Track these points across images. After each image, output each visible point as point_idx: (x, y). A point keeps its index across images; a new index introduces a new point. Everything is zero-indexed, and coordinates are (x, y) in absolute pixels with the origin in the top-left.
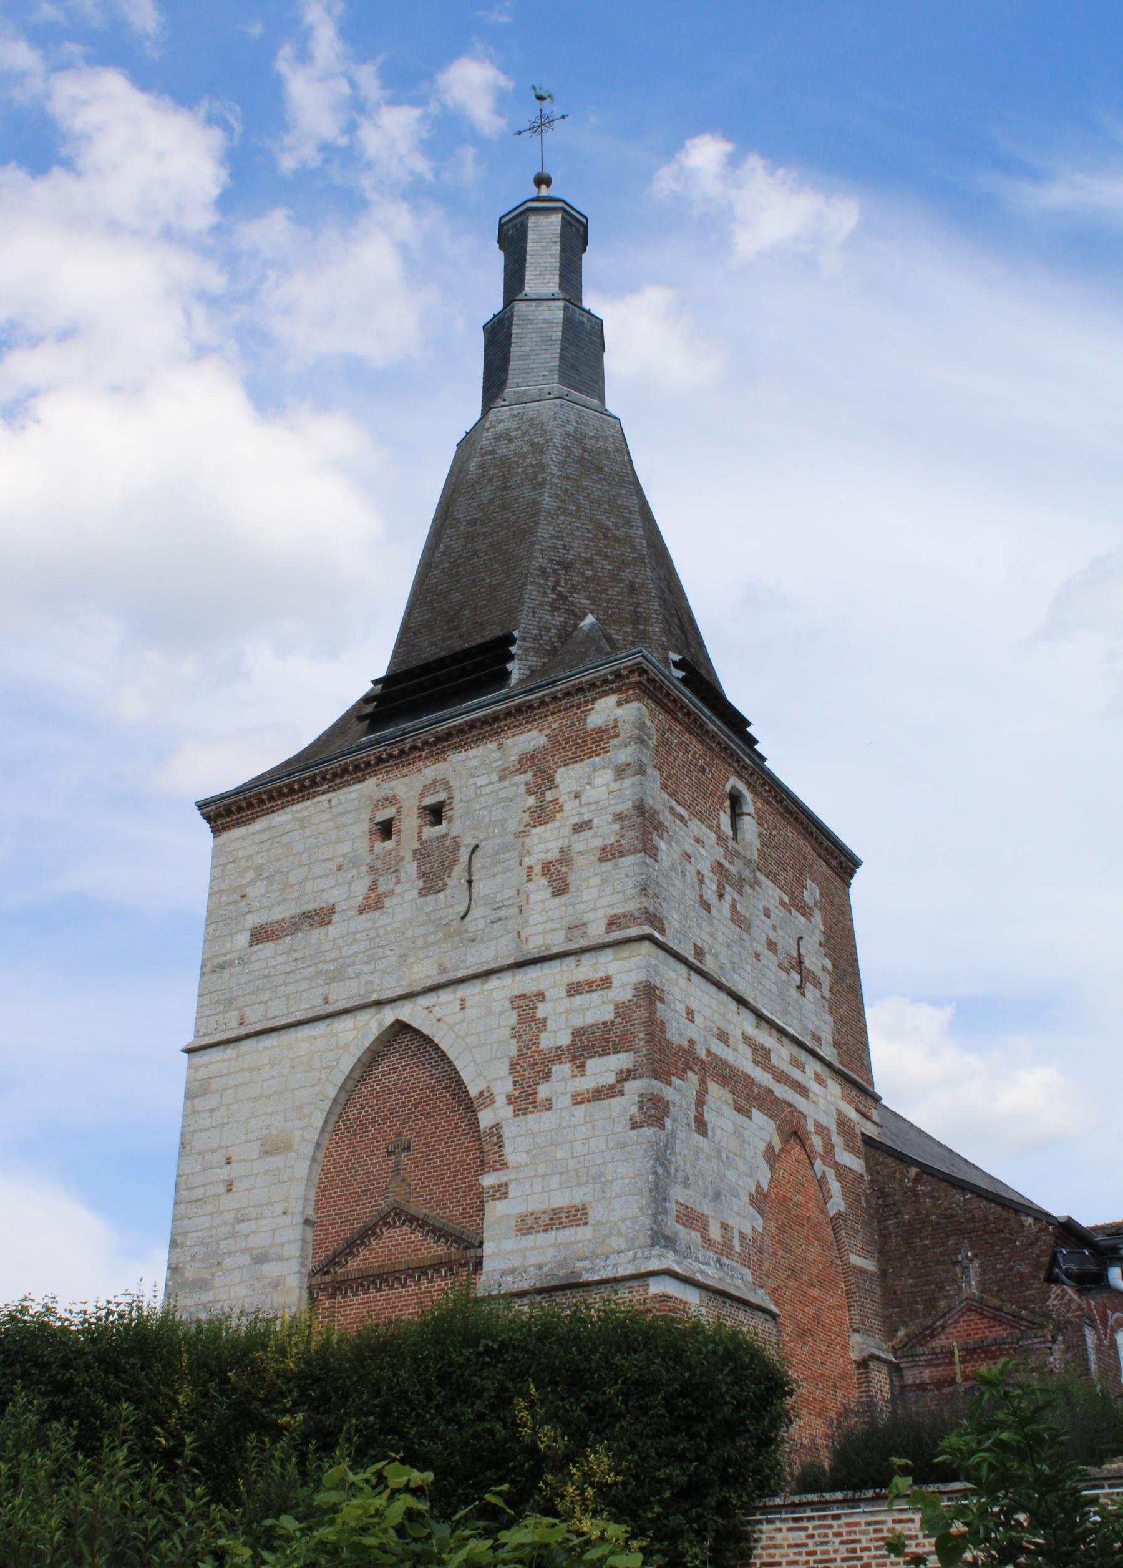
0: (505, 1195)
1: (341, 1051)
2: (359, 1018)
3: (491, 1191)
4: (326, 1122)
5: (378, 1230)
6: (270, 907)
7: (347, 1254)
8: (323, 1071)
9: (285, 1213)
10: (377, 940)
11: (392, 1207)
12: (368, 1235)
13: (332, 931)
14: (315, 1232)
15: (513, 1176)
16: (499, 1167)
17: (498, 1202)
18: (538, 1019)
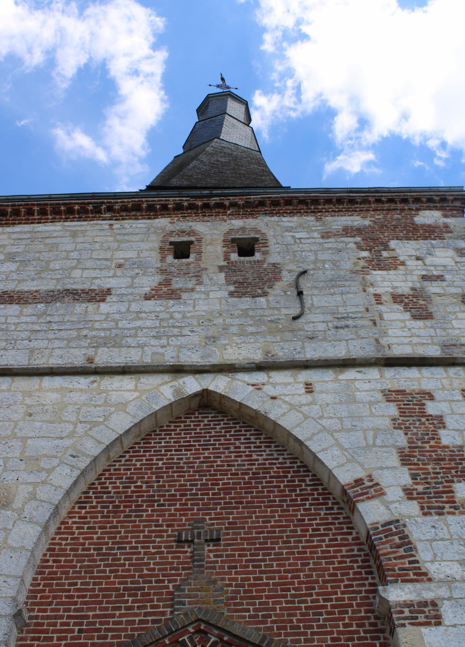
1: (113, 409)
2: (142, 380)
3: (406, 610)
4: (75, 483)
6: (20, 281)
8: (79, 425)
10: (171, 321)
11: (193, 618)
13: (104, 307)
15: (443, 592)
16: (412, 577)
17: (424, 630)
18: (430, 415)
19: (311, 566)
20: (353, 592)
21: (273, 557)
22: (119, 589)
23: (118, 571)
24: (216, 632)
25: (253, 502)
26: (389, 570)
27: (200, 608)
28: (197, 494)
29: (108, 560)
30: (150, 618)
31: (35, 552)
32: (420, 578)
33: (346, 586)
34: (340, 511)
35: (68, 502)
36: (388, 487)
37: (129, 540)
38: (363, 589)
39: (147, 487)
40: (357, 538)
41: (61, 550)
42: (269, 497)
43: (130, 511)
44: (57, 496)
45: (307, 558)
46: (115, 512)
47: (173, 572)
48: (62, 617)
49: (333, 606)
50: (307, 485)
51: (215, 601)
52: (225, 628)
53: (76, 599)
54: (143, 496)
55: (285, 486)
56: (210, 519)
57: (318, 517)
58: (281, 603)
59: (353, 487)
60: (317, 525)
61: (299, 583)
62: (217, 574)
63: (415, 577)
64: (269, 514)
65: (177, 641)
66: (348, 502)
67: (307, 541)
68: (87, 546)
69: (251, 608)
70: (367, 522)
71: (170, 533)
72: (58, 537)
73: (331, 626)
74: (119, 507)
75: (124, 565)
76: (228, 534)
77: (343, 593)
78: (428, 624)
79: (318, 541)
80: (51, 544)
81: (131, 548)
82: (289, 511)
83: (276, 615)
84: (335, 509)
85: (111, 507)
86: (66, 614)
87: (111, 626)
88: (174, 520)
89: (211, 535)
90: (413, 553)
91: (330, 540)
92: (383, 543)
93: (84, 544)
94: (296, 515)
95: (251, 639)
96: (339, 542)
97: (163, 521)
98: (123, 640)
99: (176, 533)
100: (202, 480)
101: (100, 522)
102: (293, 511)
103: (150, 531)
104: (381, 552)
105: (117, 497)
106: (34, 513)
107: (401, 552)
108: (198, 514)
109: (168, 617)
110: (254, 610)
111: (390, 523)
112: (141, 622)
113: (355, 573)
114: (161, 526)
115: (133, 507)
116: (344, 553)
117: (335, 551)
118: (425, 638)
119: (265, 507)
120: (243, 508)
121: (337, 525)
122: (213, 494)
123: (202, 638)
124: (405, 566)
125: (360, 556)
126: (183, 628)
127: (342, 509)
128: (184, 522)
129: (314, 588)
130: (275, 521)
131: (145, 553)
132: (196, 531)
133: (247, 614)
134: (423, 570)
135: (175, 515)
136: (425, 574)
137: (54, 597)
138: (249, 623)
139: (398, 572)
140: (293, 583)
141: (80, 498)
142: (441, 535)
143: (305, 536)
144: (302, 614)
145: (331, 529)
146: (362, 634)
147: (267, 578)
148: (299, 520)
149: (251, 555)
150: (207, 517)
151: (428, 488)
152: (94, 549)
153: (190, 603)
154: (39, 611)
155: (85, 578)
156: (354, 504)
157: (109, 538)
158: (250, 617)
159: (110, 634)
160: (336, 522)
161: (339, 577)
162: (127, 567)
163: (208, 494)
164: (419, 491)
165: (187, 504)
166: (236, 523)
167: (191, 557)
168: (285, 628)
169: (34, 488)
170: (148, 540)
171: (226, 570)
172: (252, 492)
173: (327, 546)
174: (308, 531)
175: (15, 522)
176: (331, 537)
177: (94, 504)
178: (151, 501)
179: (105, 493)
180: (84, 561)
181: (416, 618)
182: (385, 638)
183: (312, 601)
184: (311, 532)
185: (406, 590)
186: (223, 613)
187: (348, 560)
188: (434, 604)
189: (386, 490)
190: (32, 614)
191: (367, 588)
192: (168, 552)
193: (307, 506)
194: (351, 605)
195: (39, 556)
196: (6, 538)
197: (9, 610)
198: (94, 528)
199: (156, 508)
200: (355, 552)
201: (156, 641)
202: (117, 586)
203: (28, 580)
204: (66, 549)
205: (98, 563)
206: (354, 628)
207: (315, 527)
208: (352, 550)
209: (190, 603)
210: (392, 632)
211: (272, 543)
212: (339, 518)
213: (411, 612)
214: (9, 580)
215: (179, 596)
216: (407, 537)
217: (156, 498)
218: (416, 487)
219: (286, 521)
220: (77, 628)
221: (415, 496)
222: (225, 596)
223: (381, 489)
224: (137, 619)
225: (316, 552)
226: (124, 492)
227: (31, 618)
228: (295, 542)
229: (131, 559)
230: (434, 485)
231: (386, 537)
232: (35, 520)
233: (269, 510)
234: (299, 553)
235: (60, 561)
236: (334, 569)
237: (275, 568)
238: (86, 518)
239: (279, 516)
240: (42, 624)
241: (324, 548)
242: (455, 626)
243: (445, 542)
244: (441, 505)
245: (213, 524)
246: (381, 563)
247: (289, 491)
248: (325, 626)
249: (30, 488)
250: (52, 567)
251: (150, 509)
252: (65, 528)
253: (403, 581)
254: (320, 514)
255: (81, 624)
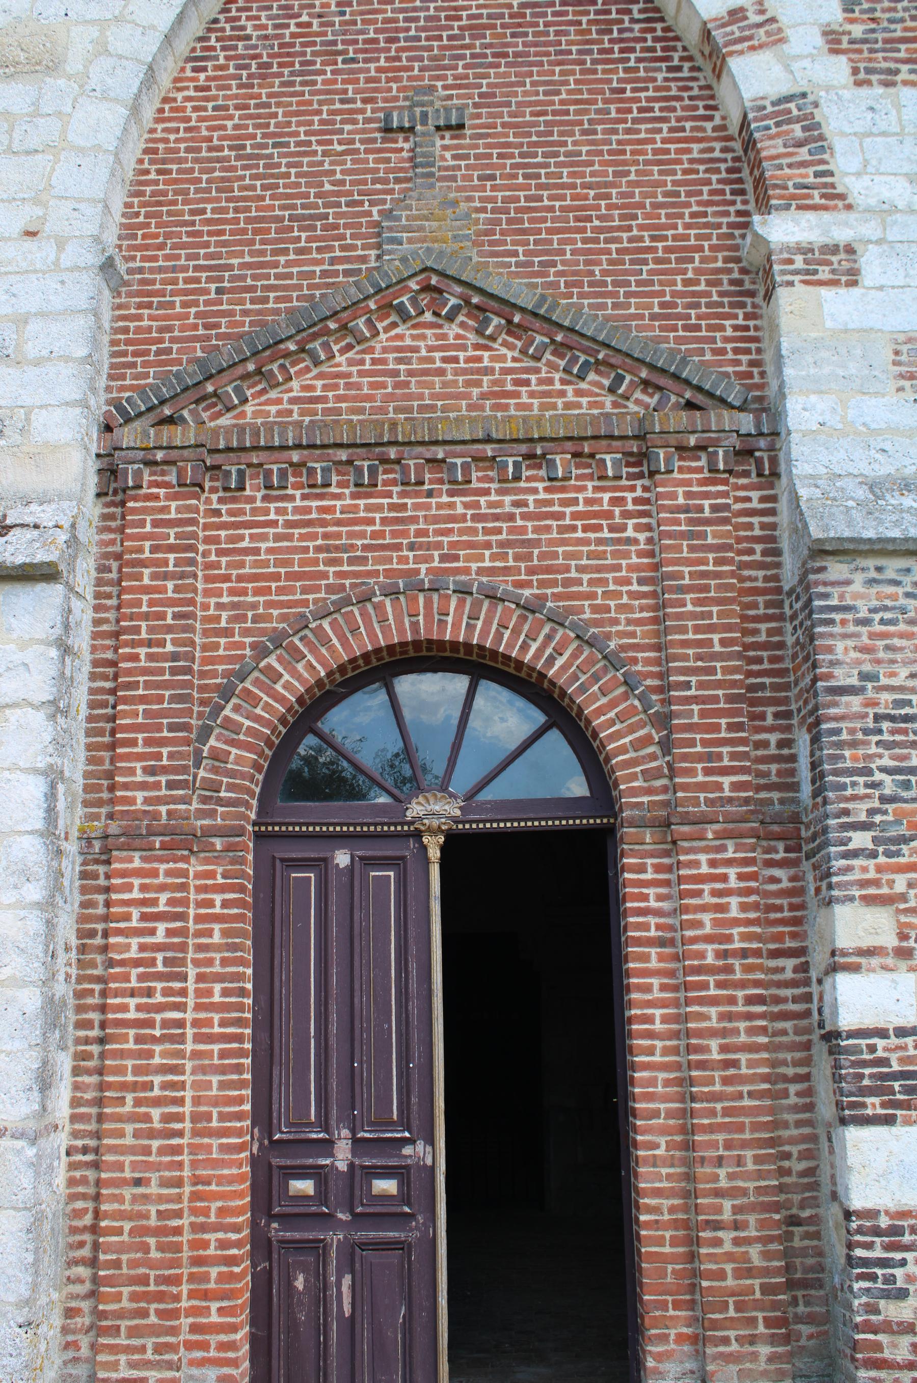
0: (852, 278)
4: (180, 19)
5: (361, 322)
7: (246, 376)
9: (31, 234)
12: (327, 332)
14: (120, 307)
15: (870, 230)
16: (817, 200)
17: (824, 291)
19: (633, 177)
20: (706, 225)
21: (562, 158)
22: (281, 219)
23: (277, 186)
24: (458, 289)
25: (528, 54)
26: (776, 186)
27: (428, 248)
28: (419, 39)
29: (257, 166)
30: (340, 267)
31: (121, 156)
32: (832, 203)
33: (693, 215)
34: (695, 74)
35: (170, 59)
36: (794, 26)
37: (294, 128)
38: (725, 220)
39: (322, 25)
40: (723, 128)
41: (169, 150)
42: (559, 43)
43: (292, 74)
44: (150, 47)
45: (624, 163)
46: (263, 77)
47: (378, 186)
48: (185, 269)
49: (667, 250)
50: (632, 21)
51: (455, 237)
52: (474, 282)
53: (206, 238)
54: (314, 44)
55: (589, 22)
56: (445, 87)
57: (651, 85)
58: (573, 241)
59: (724, 25)
60: (649, 100)
61: (609, 207)
62: (459, 189)
63: (823, 201)
64: (556, 78)
65: (391, 305)
66: (710, 55)
67: (628, 131)
68: (215, 142)
69: (520, 249)
70: (745, 96)
71: (369, 114)
72: (160, 127)
73: (661, 283)
74: (269, 65)
75: (287, 175)
76: (479, 116)
77: (687, 226)
78: (834, 283)
79: (648, 131)
80: (149, 141)
81: (298, 144)
82: (595, 72)
83: (564, 263)
84: (686, 69)
85: (254, 66)
86: (192, 263)
87: (272, 282)
88: (376, 90)
89: (448, 118)
90: (826, 157)
91: (671, 130)
92: (771, 138)
93: (210, 139)
94: (610, 81)
95: (519, 302)
96: (687, 134)
97: (356, 92)
98: (295, 303)
99: (381, 115)
100: (428, 9)
101: (236, 97)
102: (605, 71)
103: (331, 112)
104: (764, 154)
105: (264, 47)
106: (109, 81)
107: (803, 154)
108: (422, 78)
109: (373, 264)
110: (526, 253)
111: (789, 99)
112: (324, 274)
113: (712, 192)
114: (353, 101)
115: (297, 66)
116: (695, 155)
117: (677, 151)
118: (826, 306)
119: (550, 63)
120: (508, 65)
121: (687, 102)
122: (450, 38)
123: (433, 300)
124: (805, 181)
125: (725, 160)
126: (398, 282)
127: (699, 69)
128: (394, 93)
129: (635, 217)
130: (569, 92)
131: (325, 153)
132: (418, 110)
133: (513, 260)
134: (840, 190)
135: (376, 80)
136: (842, 197)
137: (168, 236)
138: (517, 275)
139: (792, 190)
140: (598, 207)
141: (194, 50)
142: (883, 126)
143: (625, 121)
144: (611, 262)
145: (674, 109)
146: (715, 298)
147: (551, 198)
148: (614, 91)
149: (522, 155)
150: (439, 84)
151: (873, 31)
152: (231, 148)
153: (410, 241)
154: (144, 259)
155: (218, 200)
156: (724, 59)
157: (257, 126)
158: (517, 264)
159: (272, 295)
160: (685, 94)
161: (683, 199)
162: (293, 179)
163: (440, 38)
164: (853, 36)
165: (399, 59)
166: (494, 95)
167: (411, 159)
168: (580, 284)
169: (102, 32)
170: (328, 129)
171: (476, 182)
172: (526, 34)
173: (664, 141)
174: (630, 111)
175: (75, 100)
176: (673, 123)
177: (222, 61)
178: (330, 53)
179: (239, 38)
180: (213, 170)
181: (816, 272)
182: (754, 306)
183: (630, 240)
184: (635, 114)
185: (804, 224)
186: (470, 259)
187: (702, 168)
188: (850, 250)
189: (789, 32)
190: (131, 265)
191: (732, 219)
192: (367, 151)
193: (632, 64)
194: (701, 249)
195: (130, 165)
196: (64, 131)
197: (94, 259)
198: (226, 108)
199: (340, 66)
200: (717, 154)
201: (354, 304)
202: (277, 213)
203: (117, 207)
204: (178, 150)
205: (240, 173)
206: (702, 287)
207: (644, 104)
208: (712, 150)
209: (410, 241)
210: (768, 296)
211: (561, 134)
212: (691, 88)
213: (806, 262)
214: (82, 206)
215: (390, 229)
216: (818, 126)
217: (340, 47)
218: (848, 27)
219: (590, 91)
220: (213, 287)
221: (845, 45)
222: (474, 228)
223: (780, 30)
224: (318, 269)
225: (643, 152)
226: (277, 36)
227: (130, 271)
228: (605, 132)
229: (299, 165)
230: (885, 24)
231: (778, 124)
232: (112, 95)
233: (557, 69)
234: (610, 152)
235: (169, 172)
236: (674, 183)
237: (565, 180)
238: (208, 88)
239: (577, 82)
240: (153, 282)
241: (659, 145)
242: (881, 288)
243: (889, 139)
244: (892, 65)
245: (450, 97)
246: (762, 173)
247: (599, 32)
248: (651, 283)
249: (94, 32)
250: (156, 182)
251: (328, 69)
252: (172, 110)
253: (799, 208)
254: (654, 80)
255: (221, 279)
